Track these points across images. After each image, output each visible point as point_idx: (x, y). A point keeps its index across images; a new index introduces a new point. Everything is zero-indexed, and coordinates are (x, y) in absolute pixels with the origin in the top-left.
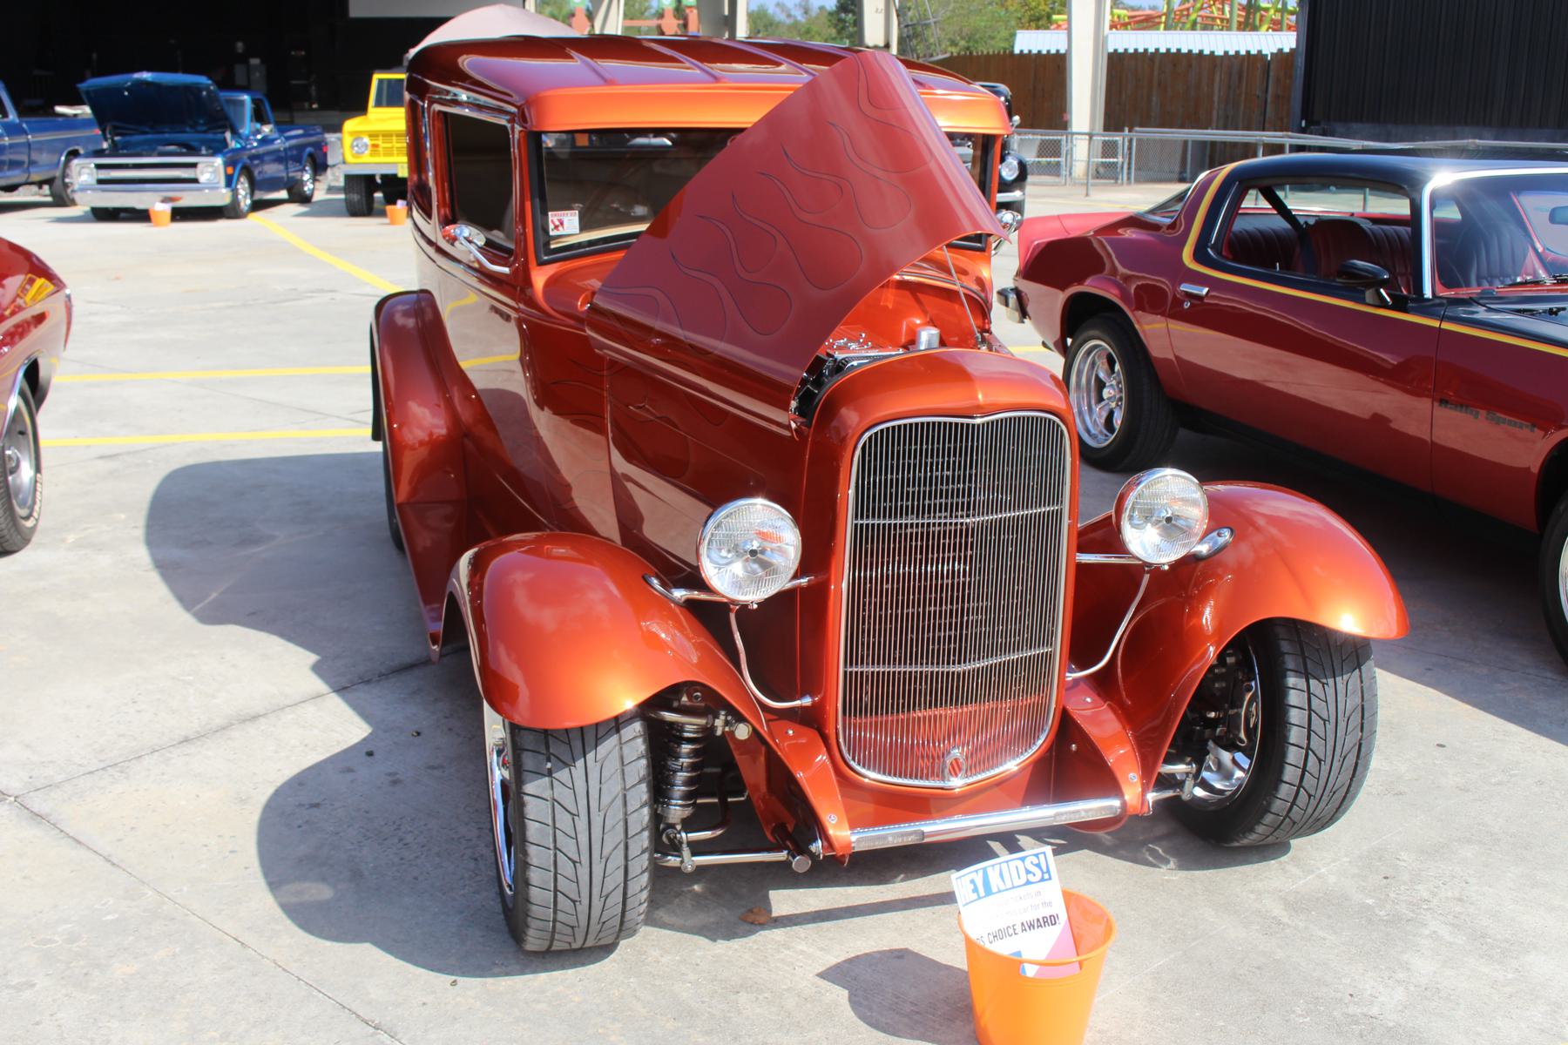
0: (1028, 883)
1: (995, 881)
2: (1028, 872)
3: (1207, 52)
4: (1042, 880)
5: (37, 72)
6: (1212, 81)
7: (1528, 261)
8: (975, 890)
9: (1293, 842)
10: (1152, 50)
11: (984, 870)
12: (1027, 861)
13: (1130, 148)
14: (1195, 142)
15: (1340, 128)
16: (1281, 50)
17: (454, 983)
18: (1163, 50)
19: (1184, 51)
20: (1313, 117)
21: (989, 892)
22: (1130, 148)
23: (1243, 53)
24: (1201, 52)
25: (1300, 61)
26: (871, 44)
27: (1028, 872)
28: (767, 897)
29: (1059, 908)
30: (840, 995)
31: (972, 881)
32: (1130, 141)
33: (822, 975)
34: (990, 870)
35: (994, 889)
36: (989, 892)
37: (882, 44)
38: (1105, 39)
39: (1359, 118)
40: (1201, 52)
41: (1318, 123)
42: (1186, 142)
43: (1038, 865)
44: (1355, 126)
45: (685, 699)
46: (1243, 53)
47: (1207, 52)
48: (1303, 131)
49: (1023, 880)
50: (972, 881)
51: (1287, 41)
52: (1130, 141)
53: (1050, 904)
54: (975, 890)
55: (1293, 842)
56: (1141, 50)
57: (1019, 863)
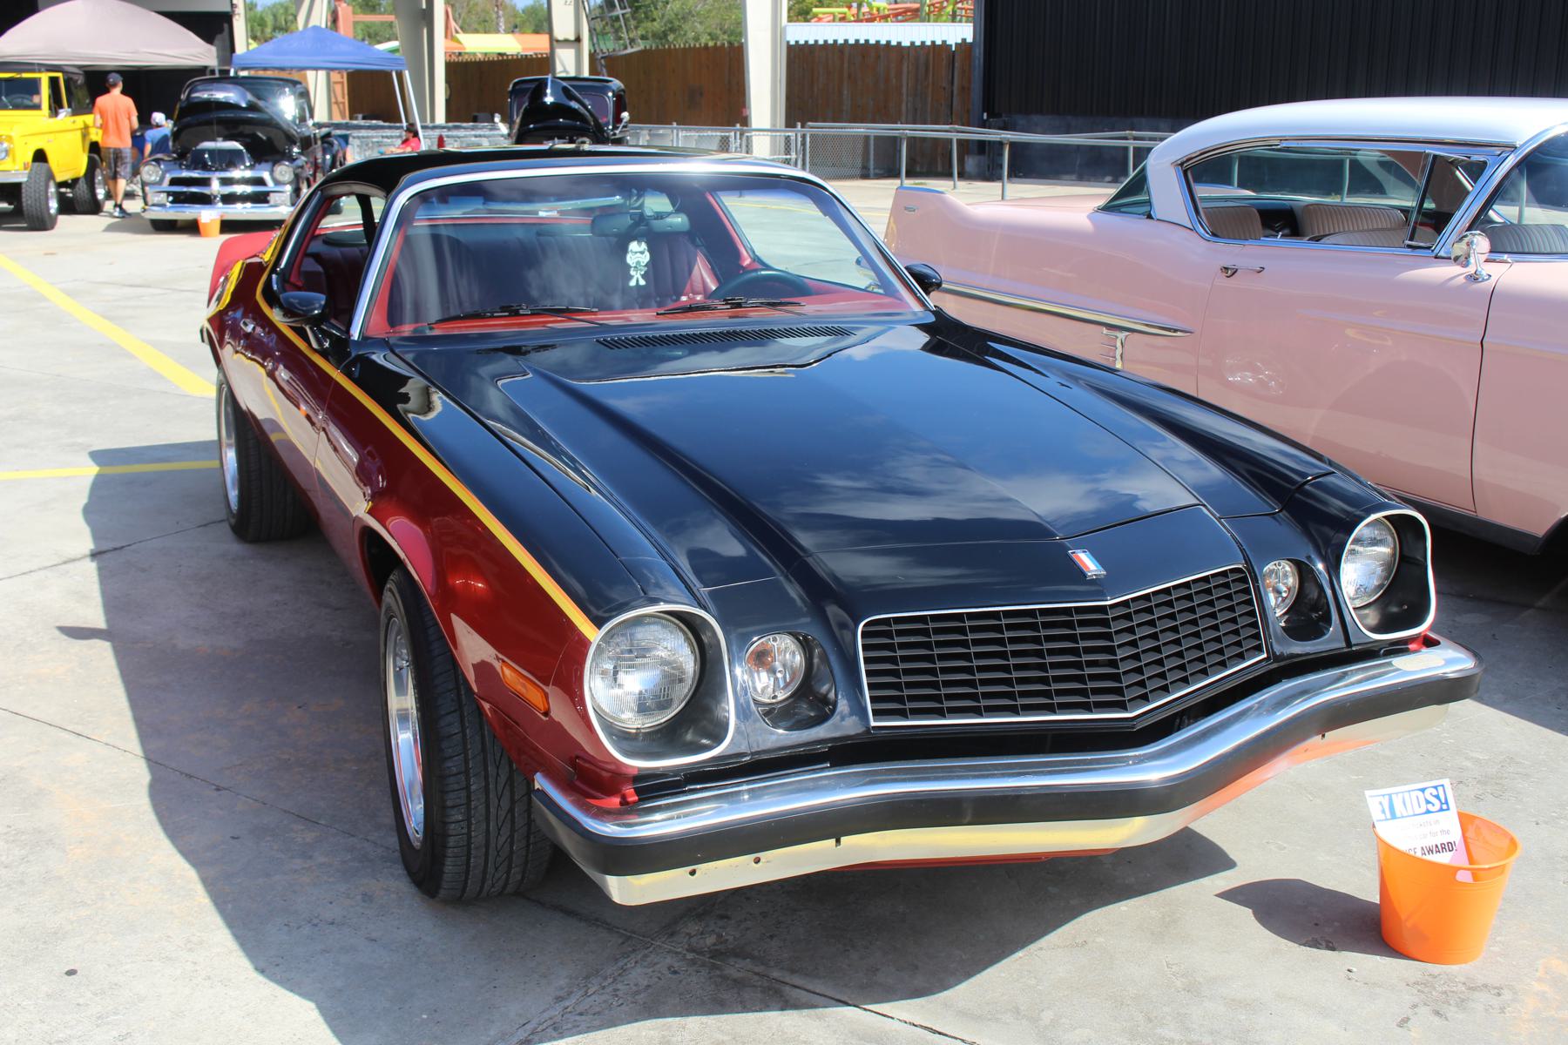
0: (1428, 812)
2: (1428, 802)
3: (894, 43)
4: (1441, 810)
6: (899, 73)
7: (695, 271)
10: (841, 41)
12: (1427, 792)
13: (804, 144)
14: (877, 138)
15: (1021, 121)
16: (964, 40)
18: (852, 41)
19: (872, 42)
20: (994, 109)
21: (1394, 816)
22: (804, 144)
23: (928, 43)
24: (888, 42)
25: (979, 52)
26: (561, 38)
29: (1455, 835)
30: (1246, 913)
32: (804, 137)
36: (1394, 816)
37: (572, 38)
38: (783, 31)
39: (1141, 114)
40: (888, 42)
41: (999, 115)
42: (867, 138)
43: (1437, 797)
44: (1036, 118)
46: (928, 43)
47: (894, 43)
48: (983, 125)
51: (959, 33)
52: (804, 137)
53: (1448, 832)
56: (831, 42)
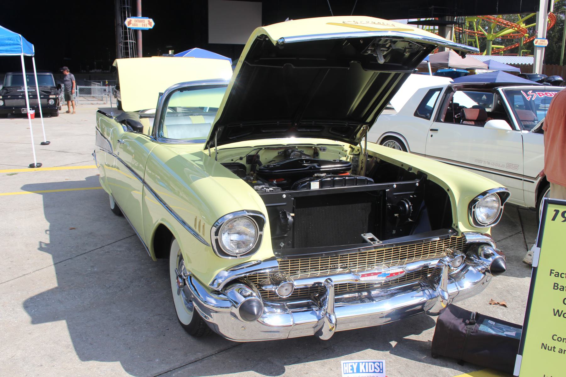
0: (374, 372)
1: (362, 367)
2: (375, 368)
4: (380, 372)
5: (65, 58)
8: (352, 369)
9: (286, 367)
11: (359, 363)
17: (68, 347)
21: (358, 371)
27: (375, 368)
28: (50, 241)
30: (38, 199)
31: (352, 366)
33: (41, 249)
34: (361, 364)
35: (361, 371)
36: (358, 371)
43: (379, 366)
45: (395, 186)
49: (373, 371)
50: (352, 366)
54: (352, 369)
55: (286, 367)
57: (373, 364)
